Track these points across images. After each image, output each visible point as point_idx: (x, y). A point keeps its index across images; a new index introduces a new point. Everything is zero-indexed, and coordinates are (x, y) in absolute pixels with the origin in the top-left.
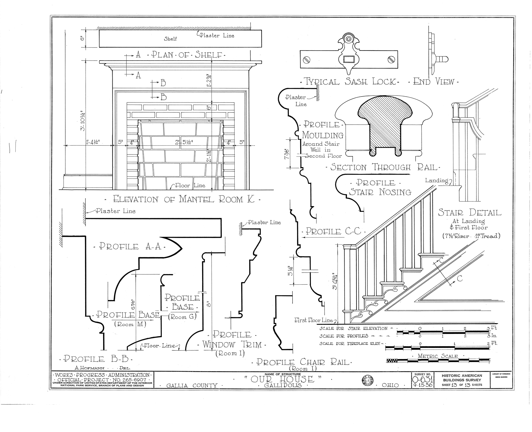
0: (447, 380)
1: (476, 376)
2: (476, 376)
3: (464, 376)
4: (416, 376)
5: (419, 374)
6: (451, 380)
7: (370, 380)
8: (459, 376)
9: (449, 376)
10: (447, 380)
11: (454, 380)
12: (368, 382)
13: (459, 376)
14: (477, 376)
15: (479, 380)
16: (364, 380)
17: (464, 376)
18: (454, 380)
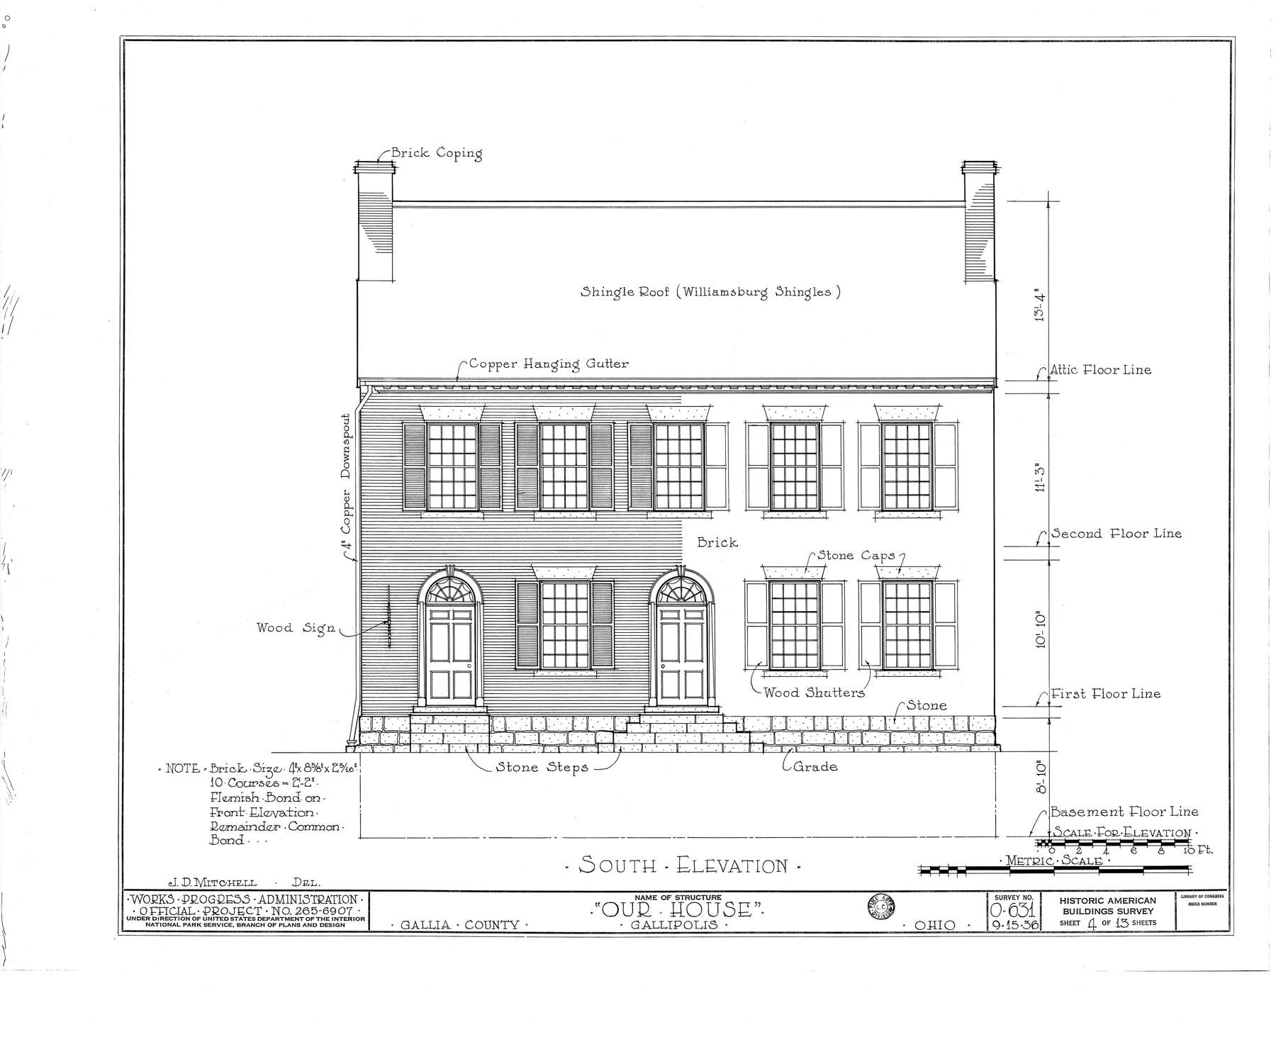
0: (1072, 912)
1: (1141, 901)
2: (1141, 901)
3: (1114, 902)
4: (999, 901)
5: (1005, 897)
6: (1083, 911)
7: (886, 907)
8: (1101, 901)
9: (1076, 901)
10: (1072, 912)
11: (1088, 911)
12: (881, 912)
13: (1101, 901)
14: (1144, 901)
15: (1148, 911)
16: (873, 906)
17: (1114, 902)
18: (1088, 911)
